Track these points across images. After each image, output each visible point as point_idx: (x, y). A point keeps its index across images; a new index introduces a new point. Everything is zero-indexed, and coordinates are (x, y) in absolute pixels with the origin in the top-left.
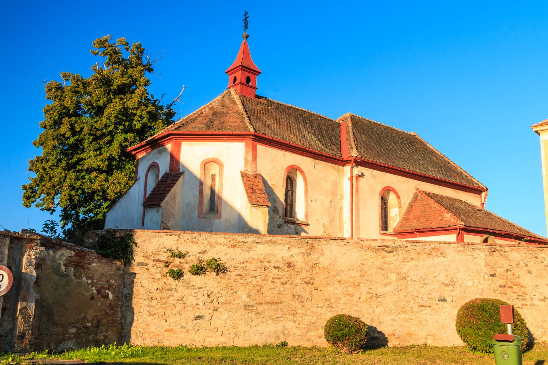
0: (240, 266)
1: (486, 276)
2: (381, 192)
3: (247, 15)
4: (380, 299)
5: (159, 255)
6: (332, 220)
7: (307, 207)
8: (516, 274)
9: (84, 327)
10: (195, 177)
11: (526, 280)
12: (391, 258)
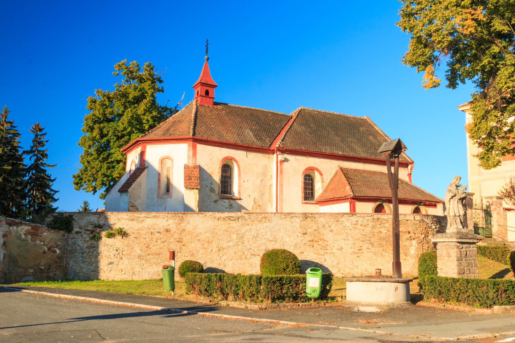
0: (136, 232)
1: (300, 235)
2: (304, 172)
4: (225, 251)
5: (88, 226)
6: (262, 195)
7: (239, 186)
8: (322, 232)
10: (155, 170)
11: (329, 236)
12: (234, 224)
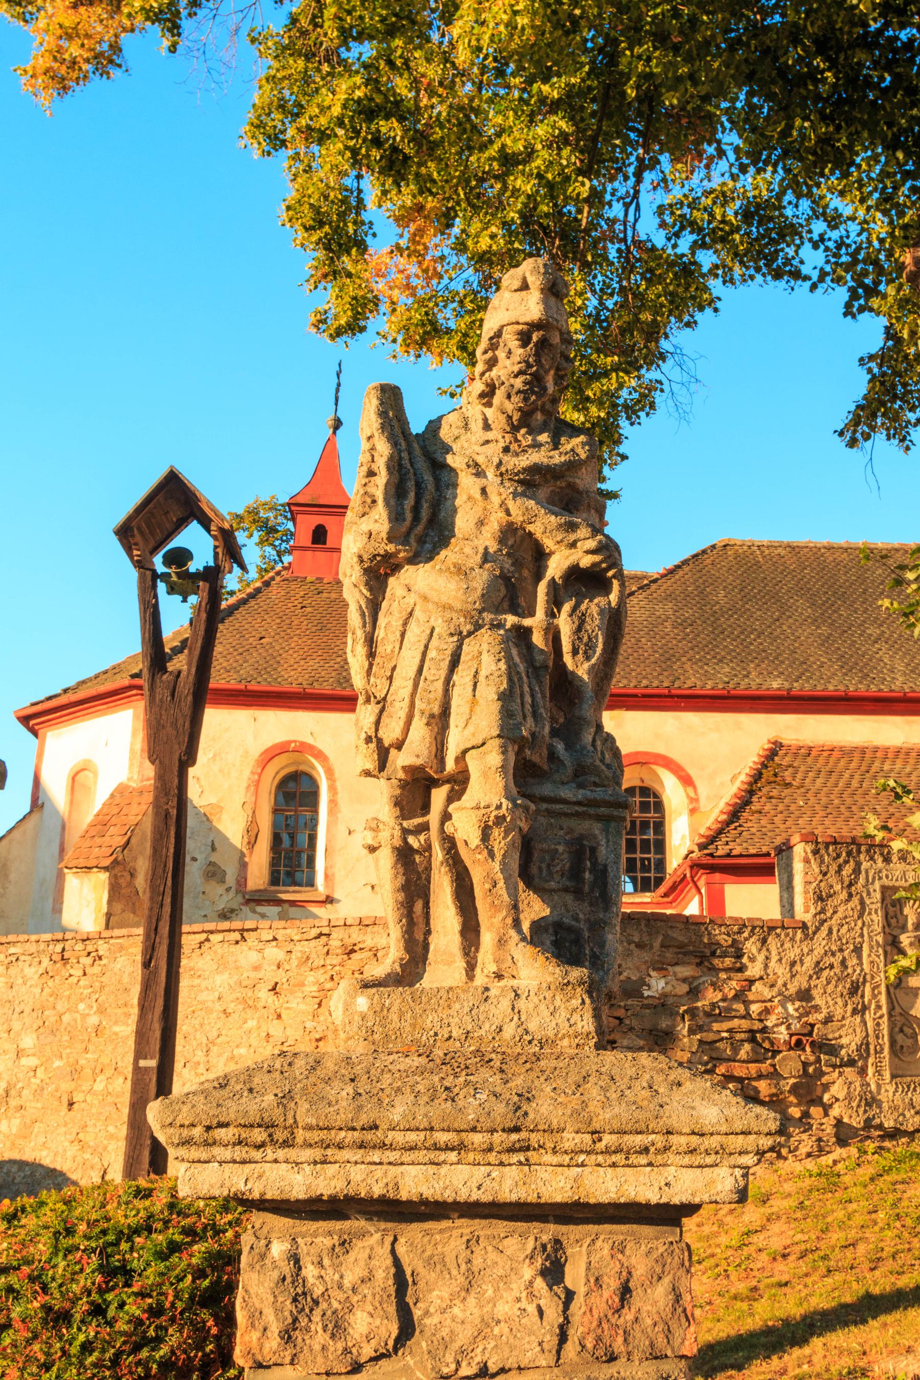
10: (56, 812)
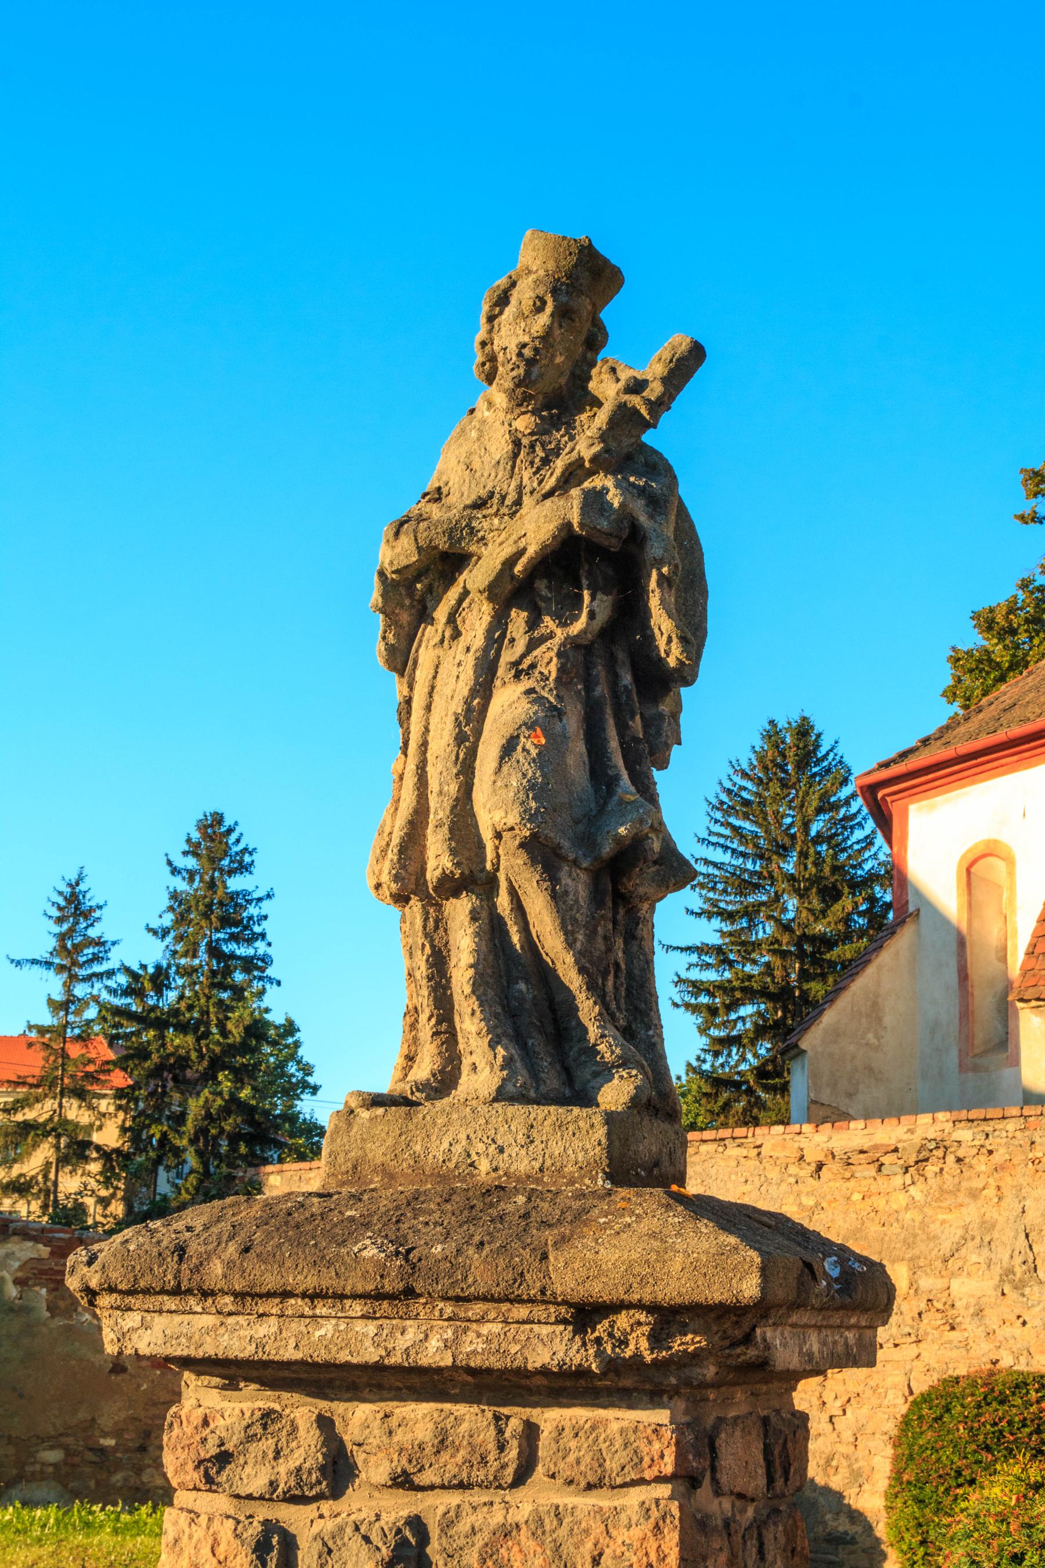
3: (634, 350)
9: (91, 1449)
10: (941, 920)
